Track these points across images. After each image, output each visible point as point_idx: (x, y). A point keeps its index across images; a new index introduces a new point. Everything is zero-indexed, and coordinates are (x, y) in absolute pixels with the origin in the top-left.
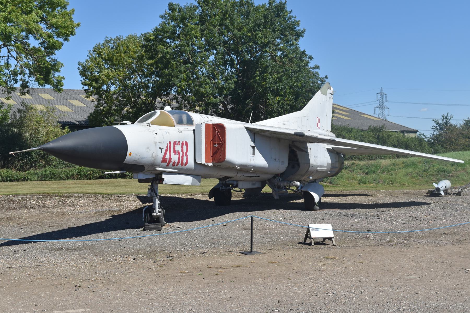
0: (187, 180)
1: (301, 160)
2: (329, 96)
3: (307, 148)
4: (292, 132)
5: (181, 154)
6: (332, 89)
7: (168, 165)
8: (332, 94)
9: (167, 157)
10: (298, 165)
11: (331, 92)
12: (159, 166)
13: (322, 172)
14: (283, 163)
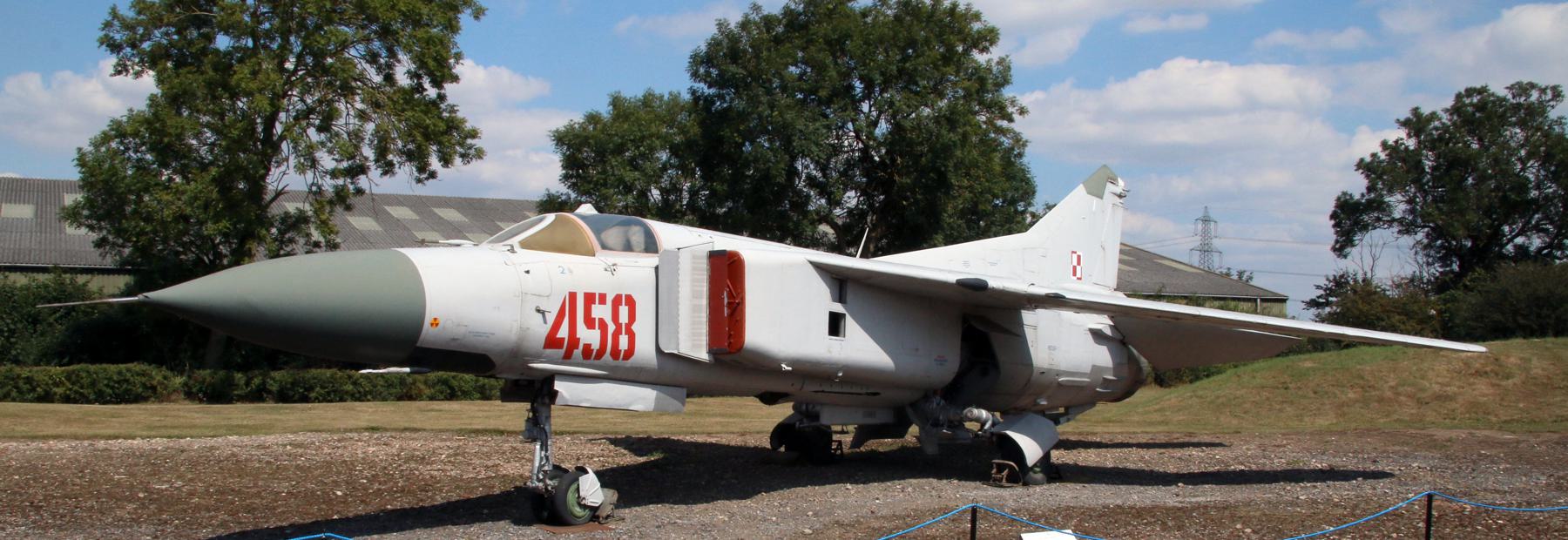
0: (642, 398)
1: (1002, 357)
2: (1109, 199)
3: (1021, 324)
4: (952, 278)
5: (611, 328)
6: (1121, 182)
7: (568, 356)
8: (1120, 196)
9: (563, 332)
10: (996, 366)
11: (1119, 190)
12: (538, 357)
13: (1077, 387)
14: (941, 360)
